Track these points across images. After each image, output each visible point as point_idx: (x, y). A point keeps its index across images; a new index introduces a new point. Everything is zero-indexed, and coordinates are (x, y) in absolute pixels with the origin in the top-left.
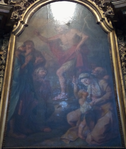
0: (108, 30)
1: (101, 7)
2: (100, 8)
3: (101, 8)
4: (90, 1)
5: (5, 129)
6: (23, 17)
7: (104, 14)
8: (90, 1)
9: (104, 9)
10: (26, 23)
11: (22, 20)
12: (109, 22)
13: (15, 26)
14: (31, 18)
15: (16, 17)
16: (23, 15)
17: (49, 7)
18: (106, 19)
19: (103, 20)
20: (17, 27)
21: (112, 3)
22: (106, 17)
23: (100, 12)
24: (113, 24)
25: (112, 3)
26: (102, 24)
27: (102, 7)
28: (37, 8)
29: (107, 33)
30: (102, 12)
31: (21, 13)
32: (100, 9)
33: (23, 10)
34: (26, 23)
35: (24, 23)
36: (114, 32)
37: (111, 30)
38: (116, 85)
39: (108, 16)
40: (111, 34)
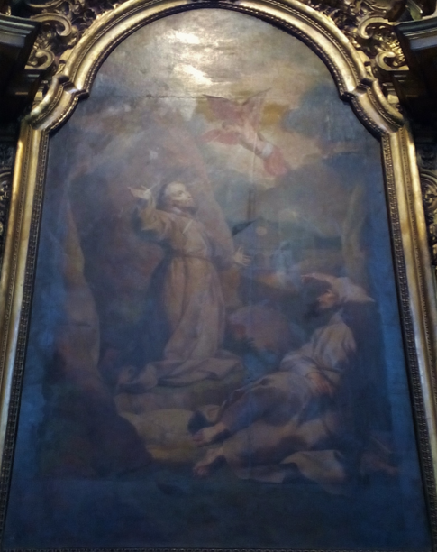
0: (382, 126)
1: (356, 39)
3: (359, 43)
7: (366, 64)
9: (369, 47)
10: (79, 86)
11: (66, 73)
12: (385, 94)
13: (39, 94)
16: (69, 56)
19: (364, 85)
22: (376, 76)
23: (358, 60)
24: (403, 105)
26: (363, 98)
27: (359, 39)
29: (377, 135)
30: (361, 58)
31: (60, 45)
33: (71, 36)
34: (79, 86)
35: (72, 85)
36: (407, 133)
39: (383, 76)
40: (394, 137)
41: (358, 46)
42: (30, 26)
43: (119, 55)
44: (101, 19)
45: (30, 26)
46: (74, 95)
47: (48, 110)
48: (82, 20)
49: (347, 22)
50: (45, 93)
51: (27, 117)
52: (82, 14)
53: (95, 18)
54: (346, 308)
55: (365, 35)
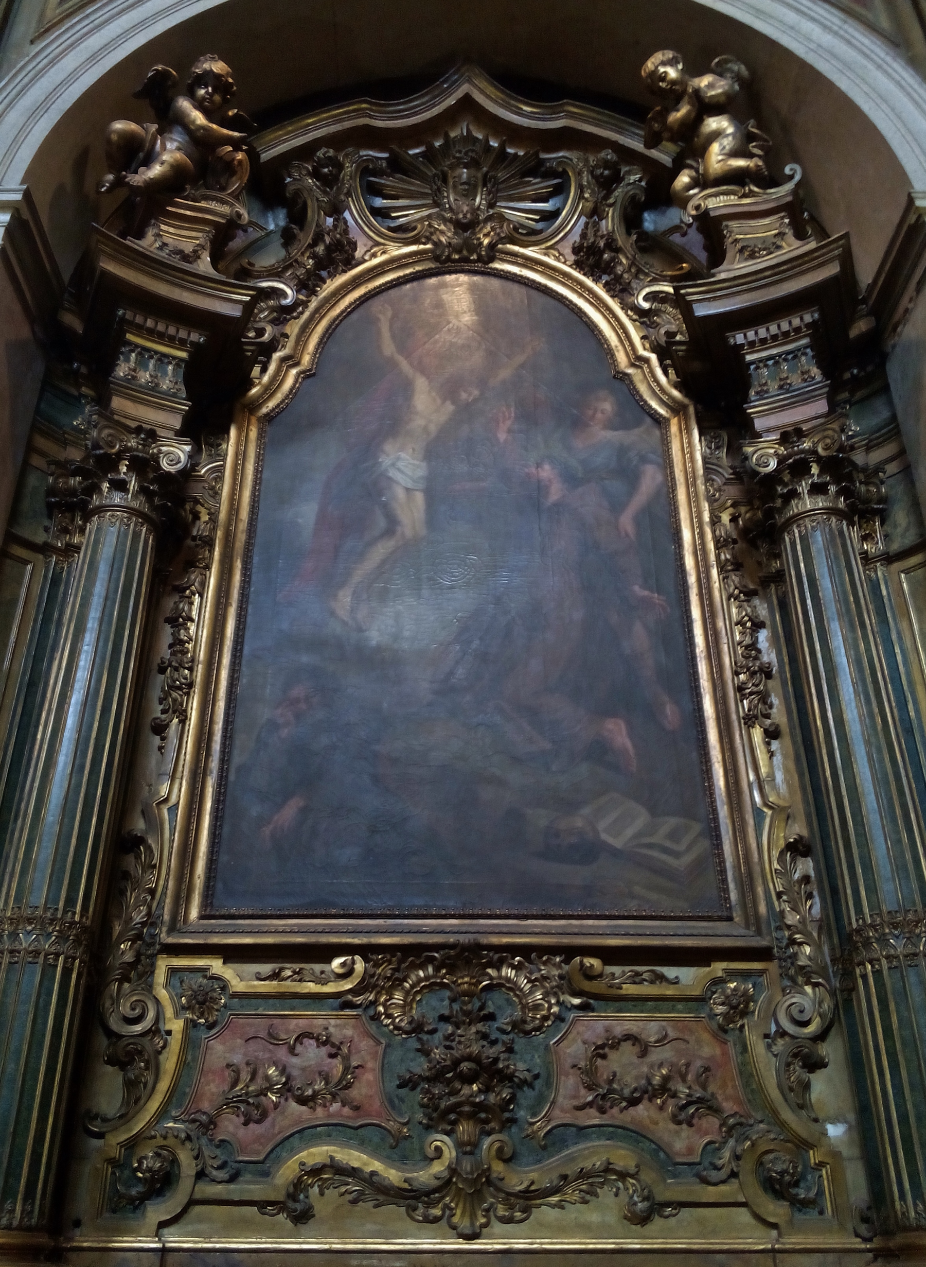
0: (662, 411)
1: (631, 310)
2: (629, 312)
3: (635, 314)
4: (7, 715)
5: (36, 1132)
6: (292, 339)
8: (810, 4)
9: (644, 317)
13: (256, 370)
14: (328, 338)
15: (263, 335)
16: (293, 328)
17: (415, 299)
18: (653, 357)
20: (266, 379)
21: (682, 291)
22: (653, 350)
25: (682, 291)
28: (355, 301)
29: (660, 422)
31: (284, 314)
32: (628, 315)
33: (296, 304)
37: (677, 409)
38: (680, 523)
39: (663, 352)
41: (635, 317)
42: (251, 292)
43: (376, 305)
44: (332, 285)
45: (251, 292)
46: (298, 374)
47: (270, 390)
48: (308, 285)
49: (620, 289)
50: (264, 370)
51: (680, 59)
52: (309, 279)
53: (325, 282)
54: (843, 965)
55: (646, 305)
